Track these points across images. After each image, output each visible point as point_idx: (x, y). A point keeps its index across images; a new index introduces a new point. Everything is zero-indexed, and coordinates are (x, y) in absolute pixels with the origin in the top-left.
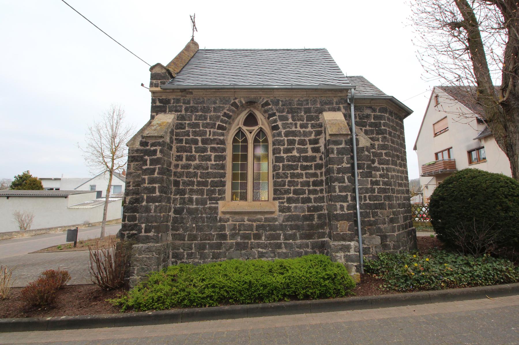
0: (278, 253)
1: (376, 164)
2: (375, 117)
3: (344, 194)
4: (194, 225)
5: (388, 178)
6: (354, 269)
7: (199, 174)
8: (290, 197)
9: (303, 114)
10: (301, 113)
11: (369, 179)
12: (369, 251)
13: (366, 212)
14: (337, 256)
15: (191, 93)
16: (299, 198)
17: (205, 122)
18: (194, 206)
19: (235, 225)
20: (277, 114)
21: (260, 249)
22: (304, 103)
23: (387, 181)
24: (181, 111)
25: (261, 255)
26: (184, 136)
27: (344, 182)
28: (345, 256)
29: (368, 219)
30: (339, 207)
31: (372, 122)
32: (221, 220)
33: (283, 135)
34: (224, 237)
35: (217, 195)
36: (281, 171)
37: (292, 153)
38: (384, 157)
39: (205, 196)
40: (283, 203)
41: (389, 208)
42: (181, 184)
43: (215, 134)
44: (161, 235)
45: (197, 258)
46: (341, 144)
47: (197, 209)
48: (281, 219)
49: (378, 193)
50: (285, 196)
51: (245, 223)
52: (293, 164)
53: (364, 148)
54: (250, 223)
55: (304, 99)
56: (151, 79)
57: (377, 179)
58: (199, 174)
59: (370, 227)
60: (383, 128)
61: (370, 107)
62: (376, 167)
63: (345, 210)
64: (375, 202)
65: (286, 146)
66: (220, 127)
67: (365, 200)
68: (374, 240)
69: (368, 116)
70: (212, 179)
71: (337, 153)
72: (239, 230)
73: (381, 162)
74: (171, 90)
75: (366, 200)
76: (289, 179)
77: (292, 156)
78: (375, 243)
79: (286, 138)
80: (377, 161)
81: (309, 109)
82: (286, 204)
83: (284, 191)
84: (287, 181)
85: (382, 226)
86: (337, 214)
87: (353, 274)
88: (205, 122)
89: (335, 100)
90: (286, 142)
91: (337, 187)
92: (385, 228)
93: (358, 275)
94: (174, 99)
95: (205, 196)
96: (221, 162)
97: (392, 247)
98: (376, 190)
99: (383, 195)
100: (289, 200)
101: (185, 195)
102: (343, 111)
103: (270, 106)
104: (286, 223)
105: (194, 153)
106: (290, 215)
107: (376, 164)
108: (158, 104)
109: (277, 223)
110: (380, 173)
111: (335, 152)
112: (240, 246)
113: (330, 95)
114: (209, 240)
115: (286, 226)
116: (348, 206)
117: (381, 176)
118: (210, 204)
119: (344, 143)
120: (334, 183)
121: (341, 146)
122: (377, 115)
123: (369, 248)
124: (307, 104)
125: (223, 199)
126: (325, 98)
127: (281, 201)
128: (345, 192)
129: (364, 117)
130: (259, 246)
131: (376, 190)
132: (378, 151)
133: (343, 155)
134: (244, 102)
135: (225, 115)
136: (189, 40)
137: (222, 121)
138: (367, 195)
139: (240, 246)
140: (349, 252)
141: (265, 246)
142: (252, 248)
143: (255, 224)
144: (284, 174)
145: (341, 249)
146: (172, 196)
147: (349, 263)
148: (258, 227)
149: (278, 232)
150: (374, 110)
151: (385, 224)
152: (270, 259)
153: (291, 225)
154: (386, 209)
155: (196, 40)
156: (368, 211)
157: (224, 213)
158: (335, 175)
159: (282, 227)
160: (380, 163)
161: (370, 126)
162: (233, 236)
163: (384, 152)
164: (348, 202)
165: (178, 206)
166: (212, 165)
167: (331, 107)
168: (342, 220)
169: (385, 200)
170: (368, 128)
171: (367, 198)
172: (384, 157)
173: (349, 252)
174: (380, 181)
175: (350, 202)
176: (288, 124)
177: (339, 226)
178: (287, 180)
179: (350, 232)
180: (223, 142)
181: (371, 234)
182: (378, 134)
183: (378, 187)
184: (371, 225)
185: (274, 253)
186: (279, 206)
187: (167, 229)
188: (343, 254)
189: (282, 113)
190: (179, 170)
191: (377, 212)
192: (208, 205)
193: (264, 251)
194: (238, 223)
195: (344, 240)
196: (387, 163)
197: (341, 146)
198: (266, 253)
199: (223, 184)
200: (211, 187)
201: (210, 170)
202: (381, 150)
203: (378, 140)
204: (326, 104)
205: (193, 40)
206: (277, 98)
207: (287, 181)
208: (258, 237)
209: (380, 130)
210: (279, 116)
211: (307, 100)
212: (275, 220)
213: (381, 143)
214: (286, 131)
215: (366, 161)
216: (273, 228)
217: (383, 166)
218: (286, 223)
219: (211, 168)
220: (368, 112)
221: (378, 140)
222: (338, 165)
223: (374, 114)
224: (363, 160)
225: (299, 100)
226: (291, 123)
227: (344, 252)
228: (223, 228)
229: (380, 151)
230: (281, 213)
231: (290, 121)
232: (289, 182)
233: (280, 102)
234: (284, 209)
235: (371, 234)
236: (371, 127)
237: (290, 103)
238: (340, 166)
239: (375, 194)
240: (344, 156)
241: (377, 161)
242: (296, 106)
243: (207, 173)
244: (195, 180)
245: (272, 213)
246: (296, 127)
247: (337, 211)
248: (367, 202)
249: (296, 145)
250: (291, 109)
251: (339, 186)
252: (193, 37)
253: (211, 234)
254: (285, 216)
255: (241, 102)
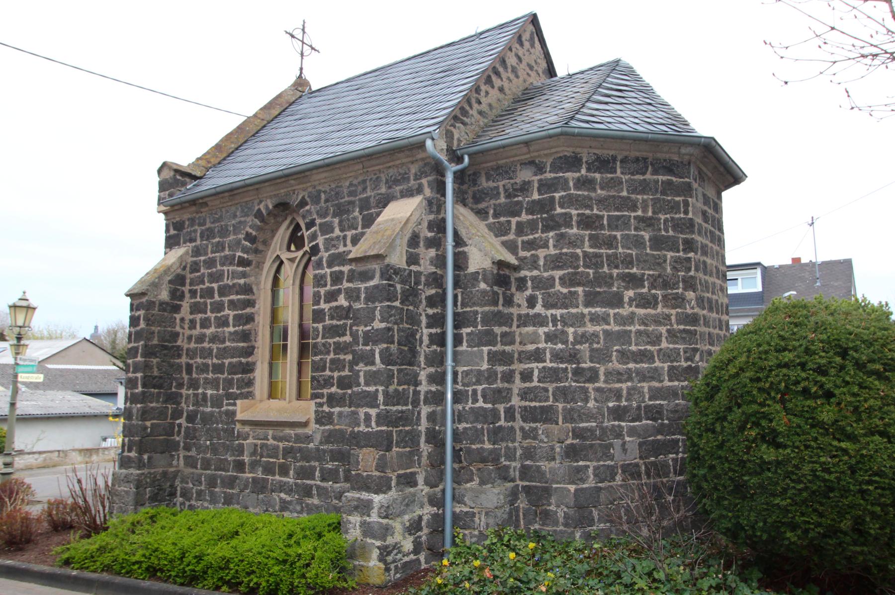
0: (307, 505)
1: (539, 309)
2: (544, 186)
3: (372, 389)
4: (208, 442)
5: (565, 342)
6: (375, 553)
7: (215, 351)
8: (331, 394)
9: (356, 213)
10: (353, 211)
11: (485, 349)
12: (473, 521)
13: (476, 430)
14: (350, 523)
15: (206, 204)
16: (345, 394)
17: (223, 254)
18: (209, 409)
19: (256, 445)
20: (318, 221)
21: (283, 495)
22: (360, 189)
23: (561, 350)
24: (195, 241)
25: (285, 506)
26: (198, 285)
27: (373, 363)
28: (363, 524)
29: (479, 446)
30: (362, 416)
31: (533, 201)
32: (239, 436)
33: (325, 265)
34: (240, 466)
35: (235, 390)
36: (319, 340)
37: (336, 300)
38: (558, 287)
39: (221, 391)
40: (320, 405)
41: (565, 420)
42: (194, 369)
43: (234, 275)
44: (149, 458)
45: (206, 500)
46: (372, 278)
47: (212, 413)
48: (318, 437)
49: (539, 381)
50: (325, 391)
51: (269, 443)
52: (338, 323)
53: (477, 273)
54: (275, 443)
55: (360, 179)
56: (160, 191)
57: (540, 346)
58: (215, 351)
59: (481, 466)
60: (559, 210)
61: (532, 163)
62: (538, 315)
63: (373, 424)
64: (533, 404)
65: (328, 287)
66: (243, 262)
67: (475, 401)
68: (483, 496)
69: (525, 188)
70: (229, 360)
71: (365, 298)
72: (262, 456)
73: (550, 300)
74: (179, 207)
75: (477, 401)
76: (332, 356)
77: (337, 307)
78: (485, 504)
79: (328, 271)
80: (540, 301)
81: (210, 230)
82: (326, 408)
83: (324, 380)
84: (328, 361)
85: (545, 465)
86: (359, 431)
87: (372, 564)
88: (223, 254)
89: (413, 171)
90: (329, 279)
91: (362, 374)
92: (552, 470)
93: (379, 568)
94: (188, 219)
95: (221, 391)
96: (241, 327)
97: (561, 520)
98: (536, 373)
99: (551, 387)
100: (332, 400)
101: (197, 389)
102: (428, 192)
103: (308, 208)
104: (325, 447)
105: (209, 314)
106: (331, 431)
107: (539, 309)
108: (172, 232)
109: (311, 445)
110: (546, 329)
111: (363, 296)
112: (259, 486)
113: (404, 161)
114: (223, 470)
115: (324, 451)
116: (378, 415)
117: (549, 338)
118: (227, 405)
119: (378, 275)
120: (357, 365)
121: (372, 283)
122: (546, 179)
123: (474, 514)
124: (364, 189)
125: (249, 395)
126: (396, 170)
127: (318, 400)
128: (375, 385)
129: (515, 190)
130: (282, 487)
131: (536, 373)
132: (546, 274)
133: (373, 302)
134: (271, 207)
135: (248, 237)
136: (292, 80)
137: (245, 250)
138: (480, 388)
139: (259, 486)
140: (369, 516)
141: (289, 491)
142: (273, 491)
143: (281, 444)
144: (324, 345)
145: (356, 508)
146: (184, 391)
147: (369, 540)
148: (287, 452)
149: (313, 463)
150: (540, 169)
151: (554, 459)
152: (296, 515)
153: (331, 451)
154: (557, 424)
155: (307, 75)
156: (479, 426)
157: (244, 423)
158: (361, 347)
159: (319, 455)
160: (546, 306)
161: (530, 212)
162: (254, 465)
163: (557, 274)
164: (378, 406)
165: (191, 408)
166: (230, 333)
167: (405, 187)
168: (366, 446)
169: (556, 400)
170: (525, 217)
171: (480, 397)
172: (558, 287)
173: (369, 516)
174: (545, 349)
175: (382, 407)
176: (332, 239)
177: (361, 457)
178: (332, 356)
179: (378, 474)
180: (247, 289)
181: (482, 483)
182: (547, 228)
183: (541, 365)
184: (483, 460)
185: (301, 504)
186: (316, 412)
187: (175, 446)
188: (359, 519)
189: (325, 217)
190: (193, 345)
191: (536, 429)
192: (224, 408)
193: (288, 498)
194: (259, 442)
195: (368, 489)
196: (567, 301)
197: (372, 283)
198: (290, 503)
199: (248, 368)
200: (229, 374)
201: (228, 344)
202: (553, 269)
203: (546, 246)
204: (397, 182)
205: (300, 77)
206: (318, 188)
207: (328, 361)
208: (284, 471)
209: (552, 218)
210: (320, 225)
211: (364, 181)
212: (308, 438)
213: (552, 251)
214: (329, 255)
215: (482, 306)
216: (307, 456)
217: (553, 311)
218: (325, 447)
219: (229, 340)
220: (525, 175)
221: (546, 246)
222: (366, 326)
223: (538, 177)
224: (474, 304)
225: (351, 185)
226: (338, 237)
227: (362, 515)
228: (240, 450)
229: (550, 273)
230: (318, 426)
231: (337, 232)
232: (333, 361)
233: (323, 196)
234: (323, 417)
235: (482, 483)
236: (532, 214)
237: (337, 193)
238: (369, 328)
239: (533, 384)
240: (377, 304)
241: (540, 301)
242: (347, 199)
243: (225, 348)
244: (210, 362)
245: (305, 424)
246: (345, 245)
247: (359, 425)
248: (478, 405)
249: (344, 282)
250: (339, 206)
251: (365, 372)
252: (301, 69)
253: (226, 460)
254: (324, 431)
255: (267, 207)
